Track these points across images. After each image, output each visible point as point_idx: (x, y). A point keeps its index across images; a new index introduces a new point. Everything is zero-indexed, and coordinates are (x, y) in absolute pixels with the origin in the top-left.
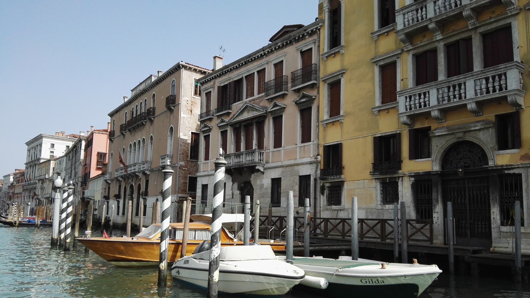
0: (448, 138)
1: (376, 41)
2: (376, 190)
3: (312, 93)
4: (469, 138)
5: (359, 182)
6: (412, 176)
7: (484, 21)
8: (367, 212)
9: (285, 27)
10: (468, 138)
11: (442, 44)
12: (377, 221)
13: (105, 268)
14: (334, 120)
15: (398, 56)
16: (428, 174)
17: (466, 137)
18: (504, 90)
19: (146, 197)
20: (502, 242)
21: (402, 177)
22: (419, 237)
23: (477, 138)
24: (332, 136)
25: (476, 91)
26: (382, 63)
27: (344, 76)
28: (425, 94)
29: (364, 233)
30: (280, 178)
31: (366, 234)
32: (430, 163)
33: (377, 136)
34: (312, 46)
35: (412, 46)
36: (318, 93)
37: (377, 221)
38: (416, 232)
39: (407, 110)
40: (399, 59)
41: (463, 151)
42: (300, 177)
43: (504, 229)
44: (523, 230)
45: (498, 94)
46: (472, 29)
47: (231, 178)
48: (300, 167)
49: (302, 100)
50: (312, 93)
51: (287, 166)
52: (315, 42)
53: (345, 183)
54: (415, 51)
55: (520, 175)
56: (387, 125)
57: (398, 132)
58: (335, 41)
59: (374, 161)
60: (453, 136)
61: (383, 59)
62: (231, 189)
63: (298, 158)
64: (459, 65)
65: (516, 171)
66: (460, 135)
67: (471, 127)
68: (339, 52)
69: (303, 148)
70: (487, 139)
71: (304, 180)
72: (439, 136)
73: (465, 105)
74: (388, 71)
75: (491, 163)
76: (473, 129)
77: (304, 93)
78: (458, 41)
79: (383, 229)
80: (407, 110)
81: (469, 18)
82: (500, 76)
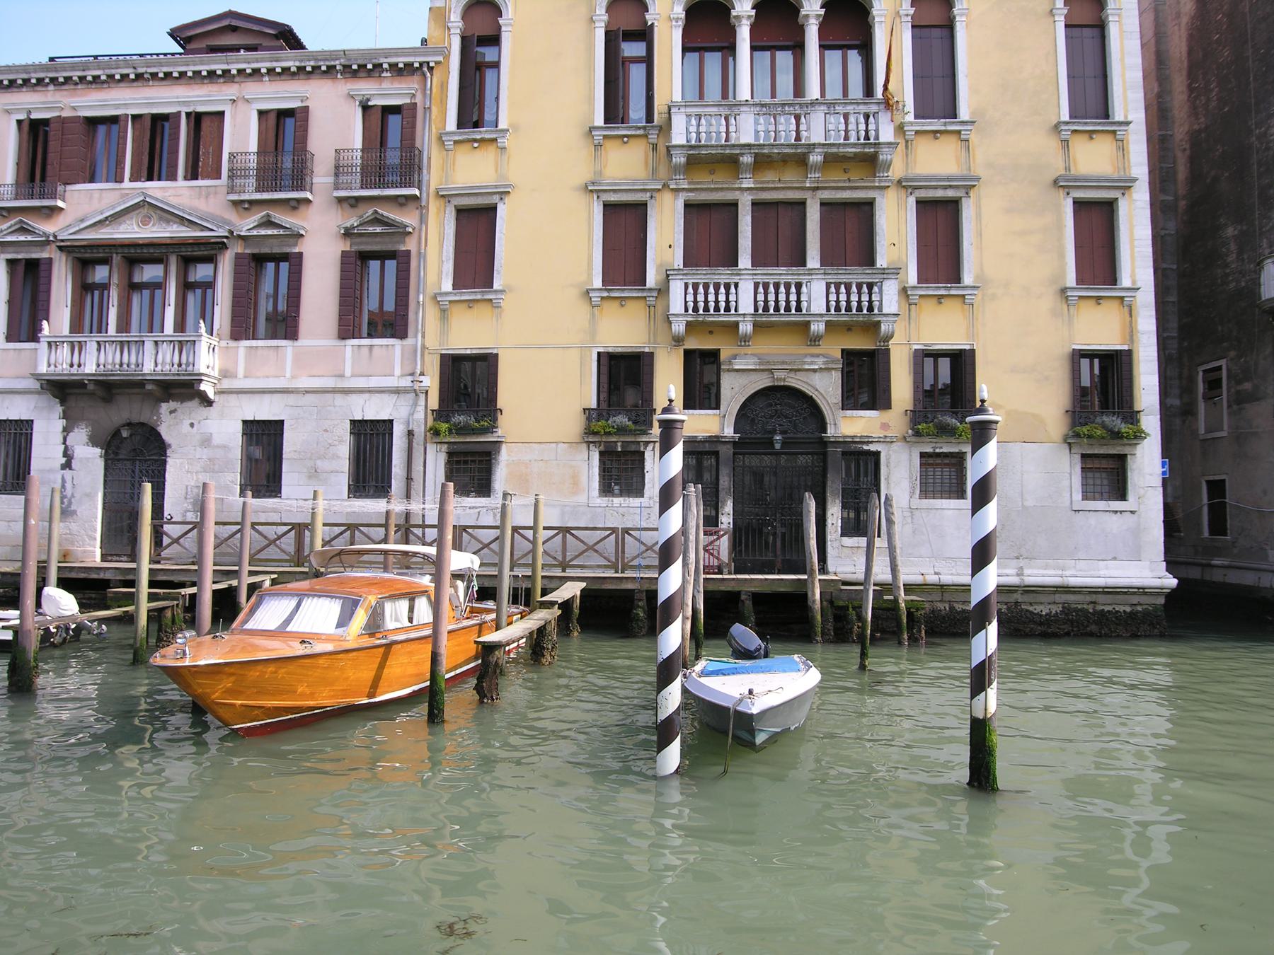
0: (754, 376)
1: (598, 146)
3: (407, 218)
4: (794, 381)
8: (563, 514)
9: (231, 14)
11: (750, 198)
12: (286, 528)
14: (479, 297)
16: (715, 440)
20: (845, 560)
24: (468, 334)
25: (828, 302)
26: (613, 198)
28: (870, 286)
29: (515, 557)
30: (282, 422)
32: (717, 419)
36: (423, 220)
37: (286, 528)
39: (686, 310)
41: (781, 407)
43: (848, 541)
45: (794, 317)
46: (809, 189)
47: (60, 409)
49: (371, 229)
50: (407, 218)
51: (308, 392)
53: (504, 447)
54: (691, 196)
55: (877, 454)
56: (624, 330)
57: (647, 350)
58: (474, 111)
59: (915, 405)
60: (765, 375)
61: (614, 191)
62: (61, 440)
63: (348, 372)
64: (780, 245)
65: (872, 448)
67: (805, 363)
68: (496, 140)
69: (365, 351)
70: (826, 388)
72: (737, 370)
74: (625, 223)
75: (831, 431)
76: (807, 367)
77: (380, 211)
79: (620, 547)
80: (686, 310)
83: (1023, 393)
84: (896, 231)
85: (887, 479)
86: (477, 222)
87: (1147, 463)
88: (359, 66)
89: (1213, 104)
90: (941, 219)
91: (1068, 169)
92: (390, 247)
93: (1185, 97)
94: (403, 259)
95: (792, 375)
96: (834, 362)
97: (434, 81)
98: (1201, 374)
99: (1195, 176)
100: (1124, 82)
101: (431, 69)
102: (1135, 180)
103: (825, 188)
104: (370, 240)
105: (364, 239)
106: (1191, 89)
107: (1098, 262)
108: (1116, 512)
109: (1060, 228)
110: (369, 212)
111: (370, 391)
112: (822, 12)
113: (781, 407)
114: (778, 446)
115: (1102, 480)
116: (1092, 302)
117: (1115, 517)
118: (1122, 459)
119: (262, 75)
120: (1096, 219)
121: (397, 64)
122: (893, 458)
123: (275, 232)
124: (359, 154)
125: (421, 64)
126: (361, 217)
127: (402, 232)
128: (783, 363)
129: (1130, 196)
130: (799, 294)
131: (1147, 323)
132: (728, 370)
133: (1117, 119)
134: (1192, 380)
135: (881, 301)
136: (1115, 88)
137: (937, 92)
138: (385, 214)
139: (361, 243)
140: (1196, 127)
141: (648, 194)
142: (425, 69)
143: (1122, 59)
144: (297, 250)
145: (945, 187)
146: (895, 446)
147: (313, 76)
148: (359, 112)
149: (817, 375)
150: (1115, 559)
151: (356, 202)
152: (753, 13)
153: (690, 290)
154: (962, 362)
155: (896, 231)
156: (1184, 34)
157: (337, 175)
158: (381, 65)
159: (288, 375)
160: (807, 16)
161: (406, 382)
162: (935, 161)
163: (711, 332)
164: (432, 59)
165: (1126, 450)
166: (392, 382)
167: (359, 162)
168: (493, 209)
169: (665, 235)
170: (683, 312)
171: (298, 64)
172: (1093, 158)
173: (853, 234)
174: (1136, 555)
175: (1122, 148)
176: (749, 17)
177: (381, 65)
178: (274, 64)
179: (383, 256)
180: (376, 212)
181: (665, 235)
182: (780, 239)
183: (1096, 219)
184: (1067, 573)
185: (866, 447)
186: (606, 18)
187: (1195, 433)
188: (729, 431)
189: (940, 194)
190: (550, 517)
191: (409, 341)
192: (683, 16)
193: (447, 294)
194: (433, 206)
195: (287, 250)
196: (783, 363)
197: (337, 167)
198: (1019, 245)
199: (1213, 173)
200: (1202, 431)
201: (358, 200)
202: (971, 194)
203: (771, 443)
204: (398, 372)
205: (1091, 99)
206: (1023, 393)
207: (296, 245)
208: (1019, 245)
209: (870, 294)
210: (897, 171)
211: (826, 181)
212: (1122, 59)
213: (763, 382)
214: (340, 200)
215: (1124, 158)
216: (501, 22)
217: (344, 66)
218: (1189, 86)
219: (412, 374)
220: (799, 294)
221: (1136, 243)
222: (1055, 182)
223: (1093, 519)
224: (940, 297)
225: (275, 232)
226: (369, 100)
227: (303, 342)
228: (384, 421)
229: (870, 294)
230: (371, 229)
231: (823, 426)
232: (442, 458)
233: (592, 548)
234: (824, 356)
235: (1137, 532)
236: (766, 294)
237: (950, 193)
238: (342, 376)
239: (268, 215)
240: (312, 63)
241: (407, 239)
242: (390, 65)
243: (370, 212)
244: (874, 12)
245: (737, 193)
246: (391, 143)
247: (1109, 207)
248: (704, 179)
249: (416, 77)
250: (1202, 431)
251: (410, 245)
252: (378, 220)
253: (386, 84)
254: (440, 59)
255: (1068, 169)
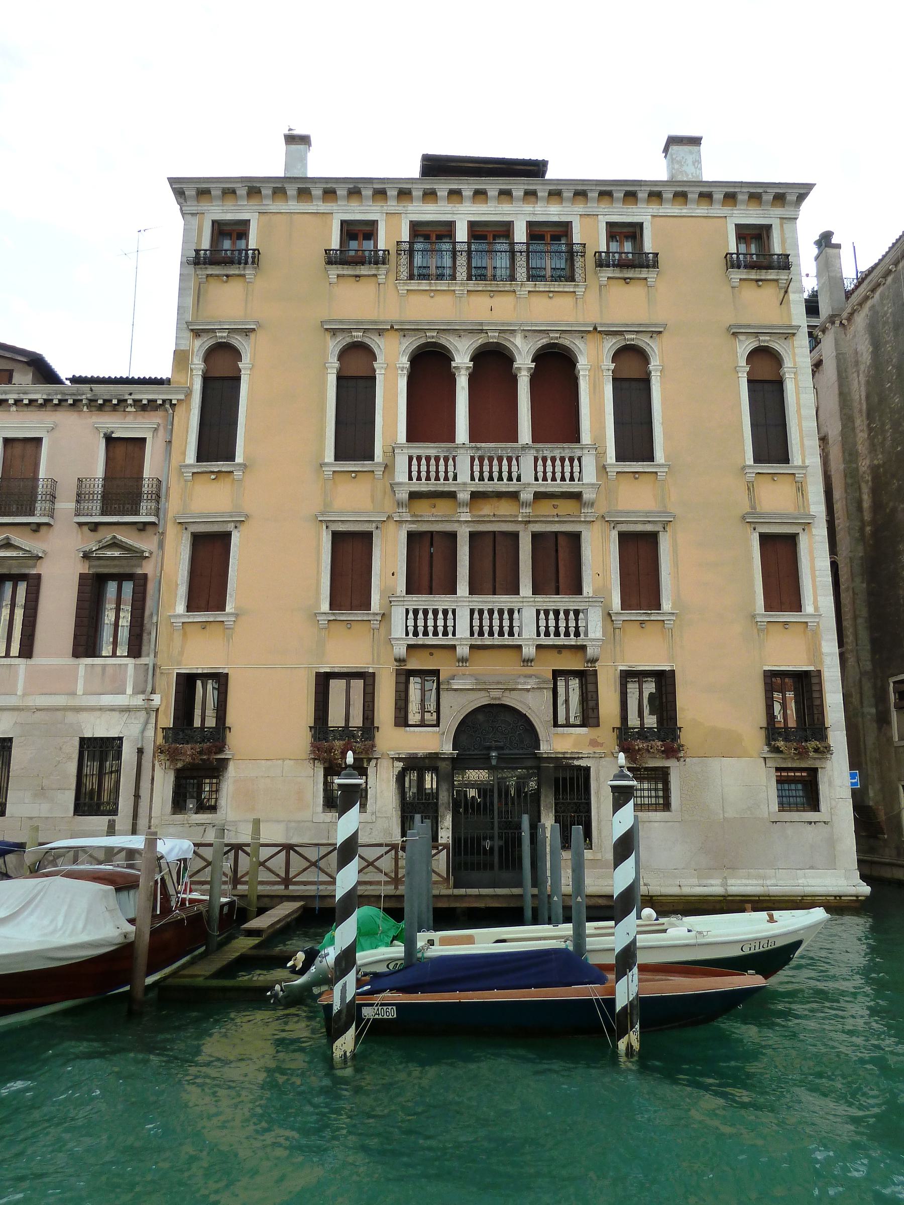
0: (473, 696)
2: (315, 783)
3: (145, 543)
5: (269, 763)
6: (399, 759)
7: (421, 516)
8: (287, 829)
10: (508, 700)
11: (468, 530)
13: (744, 1157)
15: (379, 524)
17: (504, 699)
18: (450, 636)
19: (670, 763)
21: (377, 758)
22: (264, 875)
23: (525, 704)
24: (199, 657)
27: (242, 528)
28: (577, 613)
29: (239, 875)
30: (10, 740)
31: (242, 877)
33: (322, 671)
34: (148, 435)
35: (412, 516)
36: (161, 545)
38: (368, 866)
39: (407, 634)
40: (378, 531)
41: (495, 731)
42: (83, 740)
44: (588, 854)
48: (84, 716)
49: (109, 553)
50: (145, 543)
52: (156, 430)
54: (414, 527)
55: (588, 769)
57: (371, 671)
60: (483, 694)
63: (80, 691)
65: (582, 763)
66: (494, 694)
67: (518, 683)
70: (535, 706)
71: (99, 752)
73: (454, 647)
74: (351, 552)
75: (544, 748)
76: (520, 687)
77: (119, 537)
78: (556, 534)
80: (407, 634)
81: (525, 504)
82: (577, 613)
83: (721, 709)
84: (601, 562)
85: (597, 793)
86: (211, 550)
87: (837, 779)
88: (105, 401)
89: (888, 443)
90: (640, 552)
91: (753, 507)
92: (128, 570)
93: (865, 435)
94: (141, 582)
95: (507, 693)
96: (544, 682)
97: (180, 411)
98: (892, 685)
99: (877, 506)
100: (801, 431)
101: (173, 406)
102: (814, 517)
103: (536, 522)
104: (108, 562)
105: (102, 562)
106: (870, 429)
107: (782, 589)
108: (810, 823)
109: (750, 559)
110: (107, 535)
111: (101, 709)
112: (533, 365)
113: (495, 731)
114: (494, 762)
115: (798, 790)
116: (779, 627)
117: (809, 828)
118: (813, 772)
119: (10, 406)
120: (780, 551)
121: (141, 400)
122: (602, 773)
123: (14, 554)
124: (101, 482)
125: (164, 401)
126: (100, 542)
127: (140, 556)
128: (498, 683)
129: (810, 531)
130: (511, 619)
131: (830, 647)
132: (447, 690)
133: (796, 464)
134: (885, 691)
135: (586, 627)
136: (793, 436)
137: (635, 440)
138: (124, 539)
139: (99, 566)
140: (876, 462)
141: (374, 525)
142: (168, 406)
143: (799, 411)
144: (34, 571)
145: (645, 522)
146: (603, 762)
147: (59, 408)
148: (103, 443)
149: (530, 695)
150: (812, 868)
151: (95, 527)
152: (471, 364)
153: (411, 615)
154: (665, 680)
155: (601, 562)
156: (863, 379)
157: (78, 501)
158: (126, 400)
159: (19, 693)
160: (519, 369)
161: (139, 700)
162: (636, 501)
163: (431, 654)
164: (175, 398)
165: (817, 764)
166: (119, 702)
167: (100, 490)
168: (227, 536)
169: (389, 563)
170: (404, 636)
171: (45, 397)
172: (776, 499)
173: (559, 564)
174: (831, 863)
175: (801, 489)
176: (468, 368)
177: (126, 400)
178: (22, 396)
179: (121, 578)
180: (114, 537)
181: (389, 563)
182: (494, 564)
183: (780, 551)
184: (769, 882)
185: (576, 763)
186: (337, 365)
187: (890, 739)
188: (448, 748)
189: (639, 528)
190: (272, 833)
191: (143, 660)
192: (408, 365)
193: (180, 616)
194: (171, 531)
195: (26, 571)
196: (498, 683)
197: (78, 495)
198: (708, 574)
199: (891, 504)
200: (896, 738)
201: (97, 525)
202: (668, 529)
203: (489, 758)
204: (129, 691)
205: (771, 444)
206: (721, 709)
207: (34, 566)
208: (708, 574)
209: (577, 620)
210: (602, 508)
211: (537, 516)
212: (799, 411)
213: (482, 700)
214: (80, 524)
215: (801, 495)
216: (241, 365)
217: (90, 400)
218: (869, 425)
219: (143, 692)
220: (511, 619)
221: (817, 573)
222: (744, 518)
223: (790, 830)
224: (642, 622)
225: (14, 554)
226: (113, 432)
227: (35, 661)
228: (114, 739)
229: (577, 620)
230: (109, 553)
231: (536, 743)
232: (171, 777)
233: (314, 864)
234: (537, 677)
235: (832, 842)
236: (481, 619)
237: (649, 528)
238: (74, 694)
239: (8, 538)
240: (59, 397)
241: (144, 563)
242: (134, 400)
243: (109, 537)
244: (579, 366)
245: (456, 525)
246: (123, 484)
247: (791, 540)
248: (425, 510)
249: (160, 413)
250: (896, 738)
251: (148, 568)
252: (115, 544)
253: (130, 419)
254: (182, 397)
255: (753, 507)
